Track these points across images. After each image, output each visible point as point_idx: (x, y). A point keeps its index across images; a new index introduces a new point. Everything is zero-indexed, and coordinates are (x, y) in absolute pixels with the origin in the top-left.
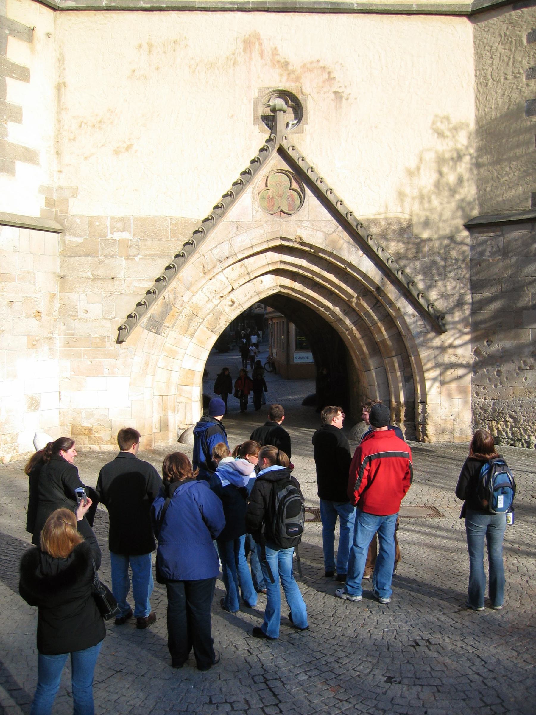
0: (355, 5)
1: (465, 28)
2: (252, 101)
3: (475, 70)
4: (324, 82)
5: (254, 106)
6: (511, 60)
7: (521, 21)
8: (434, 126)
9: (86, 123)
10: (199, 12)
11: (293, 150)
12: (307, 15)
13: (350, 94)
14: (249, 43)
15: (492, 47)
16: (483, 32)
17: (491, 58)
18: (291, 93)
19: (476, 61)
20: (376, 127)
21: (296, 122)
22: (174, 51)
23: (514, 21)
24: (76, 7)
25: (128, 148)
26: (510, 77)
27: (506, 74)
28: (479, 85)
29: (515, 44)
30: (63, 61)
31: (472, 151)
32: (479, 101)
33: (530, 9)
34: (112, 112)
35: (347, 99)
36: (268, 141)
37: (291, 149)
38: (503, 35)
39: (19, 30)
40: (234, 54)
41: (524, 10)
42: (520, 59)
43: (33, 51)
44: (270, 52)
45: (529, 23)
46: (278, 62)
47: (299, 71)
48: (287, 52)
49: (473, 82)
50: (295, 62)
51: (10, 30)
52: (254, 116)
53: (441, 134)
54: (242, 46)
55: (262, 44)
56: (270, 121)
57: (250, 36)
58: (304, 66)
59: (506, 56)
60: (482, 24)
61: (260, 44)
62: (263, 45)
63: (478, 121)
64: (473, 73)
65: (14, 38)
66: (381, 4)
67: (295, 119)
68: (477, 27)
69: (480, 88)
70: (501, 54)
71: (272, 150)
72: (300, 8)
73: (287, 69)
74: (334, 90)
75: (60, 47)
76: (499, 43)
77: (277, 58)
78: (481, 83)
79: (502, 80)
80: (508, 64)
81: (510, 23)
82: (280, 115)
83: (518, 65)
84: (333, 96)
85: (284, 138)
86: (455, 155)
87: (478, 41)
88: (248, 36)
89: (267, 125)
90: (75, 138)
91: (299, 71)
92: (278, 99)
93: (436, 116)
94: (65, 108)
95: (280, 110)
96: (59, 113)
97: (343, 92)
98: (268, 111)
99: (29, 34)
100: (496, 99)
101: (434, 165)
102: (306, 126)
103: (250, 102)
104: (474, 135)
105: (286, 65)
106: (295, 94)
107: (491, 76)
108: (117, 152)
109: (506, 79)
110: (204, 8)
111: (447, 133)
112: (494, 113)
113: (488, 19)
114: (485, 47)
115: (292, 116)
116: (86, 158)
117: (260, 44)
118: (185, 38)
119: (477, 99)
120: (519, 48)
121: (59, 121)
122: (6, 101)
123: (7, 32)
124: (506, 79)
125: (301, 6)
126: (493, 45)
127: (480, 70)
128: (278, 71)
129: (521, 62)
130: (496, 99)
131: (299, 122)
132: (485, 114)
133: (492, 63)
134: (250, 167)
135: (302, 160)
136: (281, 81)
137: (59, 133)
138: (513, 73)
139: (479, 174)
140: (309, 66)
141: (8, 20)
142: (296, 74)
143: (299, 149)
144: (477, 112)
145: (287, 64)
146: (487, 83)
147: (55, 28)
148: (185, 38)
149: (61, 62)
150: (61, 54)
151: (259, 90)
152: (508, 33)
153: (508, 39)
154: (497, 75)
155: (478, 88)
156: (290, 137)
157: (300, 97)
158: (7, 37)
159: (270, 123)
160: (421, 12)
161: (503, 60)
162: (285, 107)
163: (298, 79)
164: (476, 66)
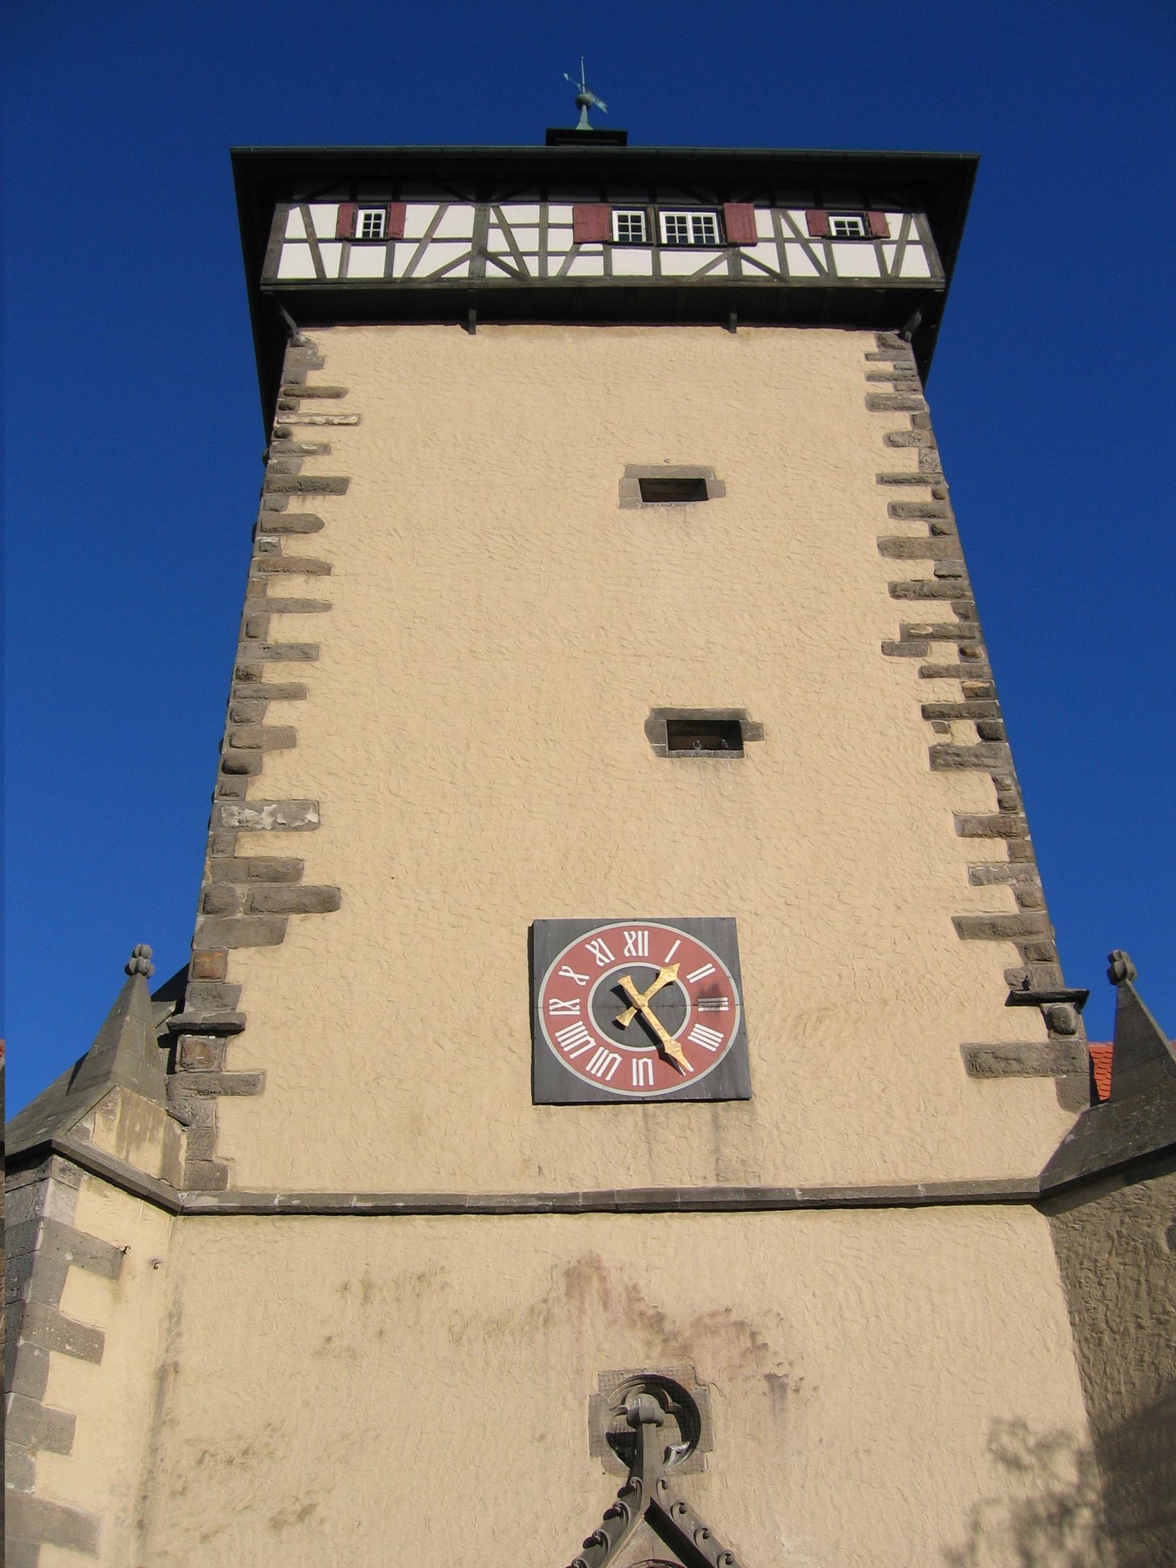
0: (798, 1193)
1: (1032, 1230)
2: (587, 1403)
3: (1070, 1312)
4: (743, 1355)
5: (590, 1413)
6: (1144, 1286)
7: (1148, 1205)
8: (994, 1446)
9: (213, 1456)
10: (473, 1216)
11: (682, 1512)
12: (699, 1216)
13: (801, 1379)
14: (579, 1276)
15: (1096, 1261)
16: (1072, 1233)
17: (1100, 1284)
18: (672, 1382)
19: (1067, 1292)
20: (867, 1451)
21: (685, 1446)
22: (418, 1296)
23: (1132, 1206)
24: (219, 1207)
25: (305, 1513)
26: (1147, 1322)
27: (1137, 1317)
28: (1083, 1343)
29: (1145, 1251)
30: (180, 1317)
31: (1092, 1496)
32: (1090, 1379)
33: (1161, 1179)
34: (274, 1430)
35: (797, 1391)
36: (622, 1493)
37: (676, 1510)
38: (1115, 1236)
39: (94, 1253)
40: (545, 1301)
41: (1149, 1182)
42: (1161, 1283)
43: (117, 1296)
44: (624, 1295)
45: (1165, 1209)
46: (642, 1314)
47: (687, 1334)
48: (660, 1292)
49: (1070, 1340)
50: (679, 1313)
51: (76, 1254)
52: (591, 1437)
53: (1014, 1464)
54: (562, 1284)
55: (605, 1278)
56: (626, 1445)
57: (579, 1261)
58: (697, 1323)
59: (1131, 1278)
60: (1068, 1216)
61: (602, 1279)
62: (608, 1280)
63: (1095, 1422)
64: (1065, 1319)
65: (81, 1270)
66: (851, 1189)
67: (684, 1440)
68: (1057, 1223)
69: (1086, 1351)
70: (1118, 1275)
71: (634, 1514)
72: (683, 1203)
73: (660, 1330)
74: (767, 1371)
75: (176, 1288)
76: (1110, 1253)
77: (639, 1307)
78: (1086, 1339)
79: (1132, 1331)
80: (1137, 1296)
81: (1126, 1210)
82: (649, 1431)
83: (1159, 1296)
84: (764, 1385)
85: (660, 1484)
86: (1054, 1509)
87: (1065, 1251)
88: (576, 1264)
89: (621, 1455)
90: (184, 1489)
91: (687, 1334)
92: (643, 1395)
93: (996, 1421)
94: (171, 1421)
95: (649, 1421)
96: (155, 1431)
97: (786, 1376)
98: (621, 1424)
99: (112, 1263)
100: (1127, 1373)
101: (1008, 1538)
102: (709, 1455)
103: (581, 1404)
104: (1092, 1459)
105: (658, 1321)
106: (681, 1383)
107: (1107, 1322)
108: (277, 1524)
109: (1140, 1327)
110: (482, 1208)
111: (1027, 1459)
112: (1128, 1404)
113: (1077, 1206)
114: (1081, 1264)
115: (677, 1432)
116: (205, 1538)
117: (602, 1279)
118: (442, 1268)
119: (1085, 1376)
120: (1156, 1261)
121: (154, 1450)
122: (43, 1404)
123: (69, 1257)
124: (1140, 1327)
125: (686, 1199)
126: (1099, 1258)
127: (1080, 1313)
128: (641, 1334)
129: (1165, 1290)
130: (1127, 1373)
131: (692, 1447)
132: (1109, 1407)
133: (1104, 1295)
134: (584, 1555)
135: (705, 1537)
136: (648, 1357)
137: (149, 1477)
138: (1152, 1313)
139: (1119, 1551)
140: (708, 1321)
141: (75, 1233)
142: (680, 1340)
143: (697, 1510)
144: (1090, 1403)
145: (660, 1318)
146: (1100, 1339)
147: (170, 1250)
148: (442, 1268)
149: (175, 1319)
150: (175, 1303)
151: (602, 1377)
152: (1125, 1232)
153: (1128, 1244)
154: (1118, 1320)
155: (1082, 1351)
156: (673, 1481)
157: (693, 1390)
158: (67, 1268)
159: (627, 1450)
160: (937, 1200)
161: (1126, 1287)
162: (659, 1413)
163: (685, 1351)
164: (1070, 1304)
